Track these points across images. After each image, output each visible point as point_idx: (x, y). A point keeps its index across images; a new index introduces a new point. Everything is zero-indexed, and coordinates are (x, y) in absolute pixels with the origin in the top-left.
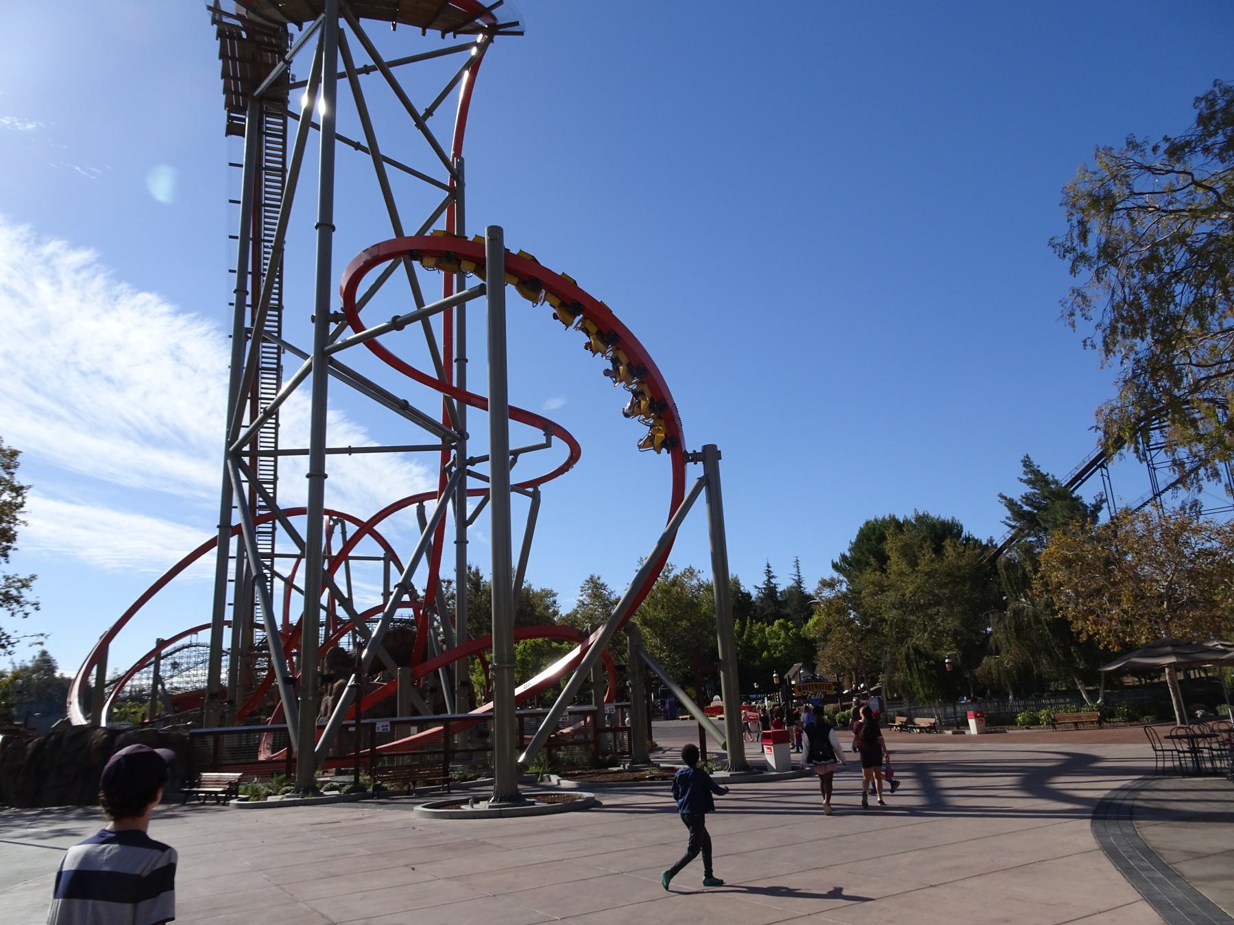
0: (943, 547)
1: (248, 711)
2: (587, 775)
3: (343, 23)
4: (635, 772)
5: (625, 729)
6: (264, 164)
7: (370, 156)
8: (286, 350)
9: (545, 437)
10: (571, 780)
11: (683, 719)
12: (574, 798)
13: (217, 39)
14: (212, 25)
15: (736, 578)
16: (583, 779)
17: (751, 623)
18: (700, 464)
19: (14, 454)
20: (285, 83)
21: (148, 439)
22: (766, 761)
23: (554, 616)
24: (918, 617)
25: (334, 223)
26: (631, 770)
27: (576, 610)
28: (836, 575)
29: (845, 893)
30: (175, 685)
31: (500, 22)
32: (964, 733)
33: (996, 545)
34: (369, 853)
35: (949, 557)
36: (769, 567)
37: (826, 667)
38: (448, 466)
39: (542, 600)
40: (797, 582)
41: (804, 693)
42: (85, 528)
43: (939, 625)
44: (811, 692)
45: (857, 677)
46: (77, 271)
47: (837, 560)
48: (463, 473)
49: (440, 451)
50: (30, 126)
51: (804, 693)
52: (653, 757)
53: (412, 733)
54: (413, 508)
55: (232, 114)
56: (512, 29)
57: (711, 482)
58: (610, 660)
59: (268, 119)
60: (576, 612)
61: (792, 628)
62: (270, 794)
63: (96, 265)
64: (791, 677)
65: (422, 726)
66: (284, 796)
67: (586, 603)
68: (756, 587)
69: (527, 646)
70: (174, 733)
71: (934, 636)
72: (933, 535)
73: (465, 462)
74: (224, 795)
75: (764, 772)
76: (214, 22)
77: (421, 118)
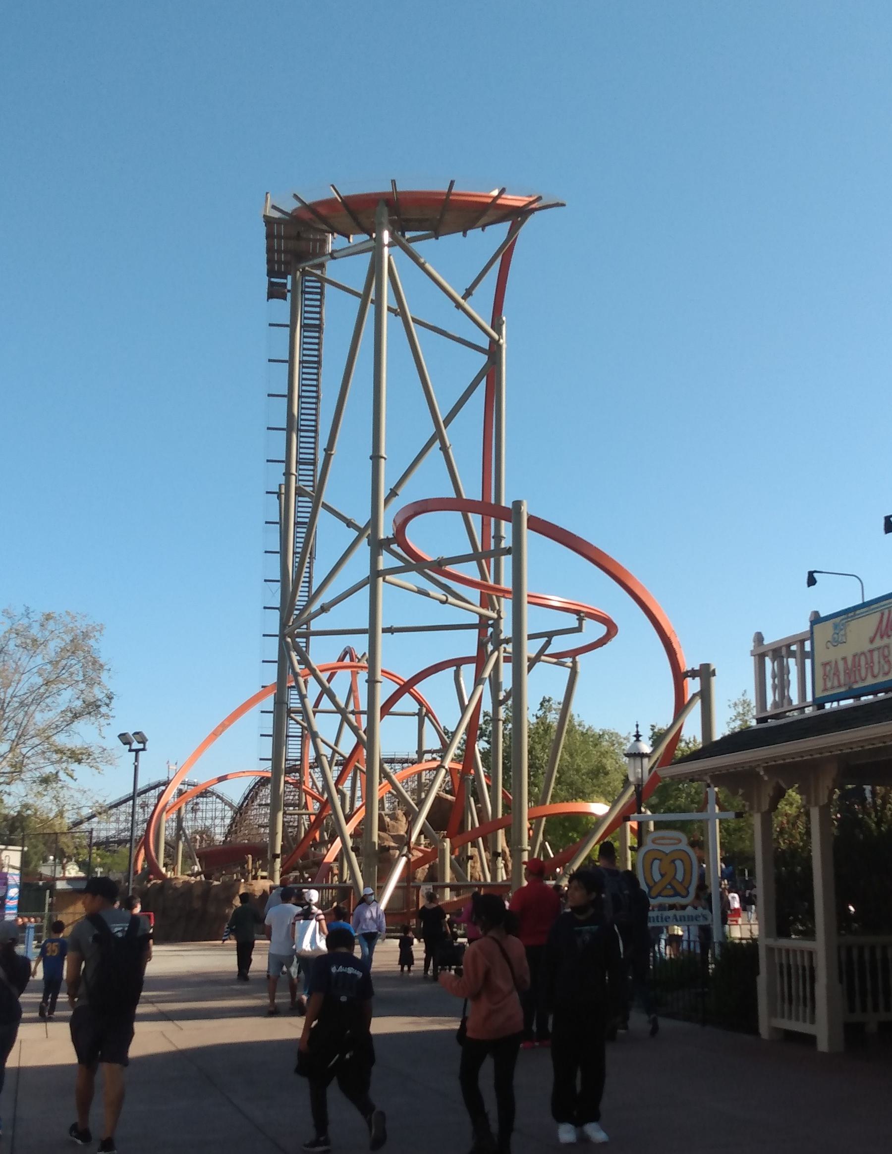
29: (822, 615)
57: (705, 694)
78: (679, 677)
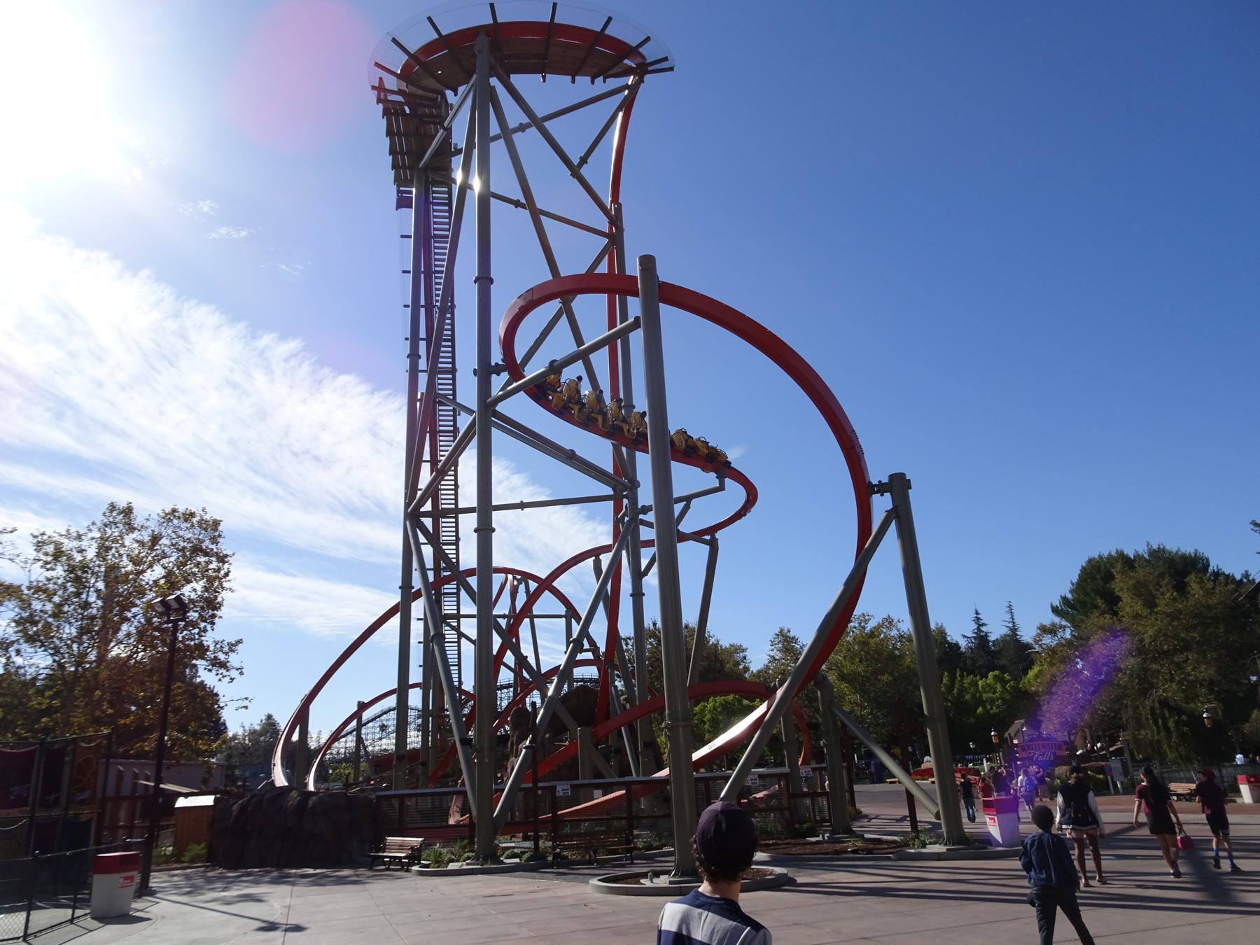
0: (1186, 584)
1: (441, 773)
2: (781, 846)
3: (494, 81)
4: (835, 843)
5: (825, 794)
6: (433, 232)
7: (528, 212)
8: (461, 412)
9: (717, 480)
10: (764, 852)
11: (891, 783)
12: (765, 873)
13: (383, 118)
14: (378, 104)
15: (941, 627)
16: (778, 851)
17: (962, 676)
18: (888, 495)
19: (216, 524)
20: (446, 151)
21: (353, 512)
22: (989, 833)
23: (745, 672)
24: (1162, 666)
25: (492, 276)
26: (832, 841)
27: (767, 666)
28: (1057, 620)
30: (384, 747)
31: (649, 60)
32: (1235, 801)
33: (1254, 580)
34: (533, 934)
35: (1195, 594)
36: (977, 613)
37: (1054, 724)
38: (621, 516)
39: (731, 656)
40: (1011, 630)
41: (1029, 753)
42: (301, 598)
43: (1189, 674)
44: (1038, 753)
45: (1092, 737)
46: (287, 360)
47: (1057, 603)
48: (636, 523)
49: (612, 502)
50: (243, 234)
51: (1029, 753)
52: (856, 827)
53: (595, 797)
54: (590, 562)
55: (401, 189)
56: (662, 65)
57: (901, 515)
58: (803, 717)
59: (434, 189)
60: (767, 667)
61: (1009, 681)
62: (452, 861)
63: (303, 353)
64: (1012, 735)
65: (607, 789)
66: (464, 863)
67: (777, 657)
68: (965, 636)
69: (717, 704)
70: (362, 795)
71: (1183, 687)
72: (1172, 570)
73: (636, 510)
74: (407, 861)
75: (988, 847)
76: (379, 101)
77: (576, 166)
78: (864, 490)
